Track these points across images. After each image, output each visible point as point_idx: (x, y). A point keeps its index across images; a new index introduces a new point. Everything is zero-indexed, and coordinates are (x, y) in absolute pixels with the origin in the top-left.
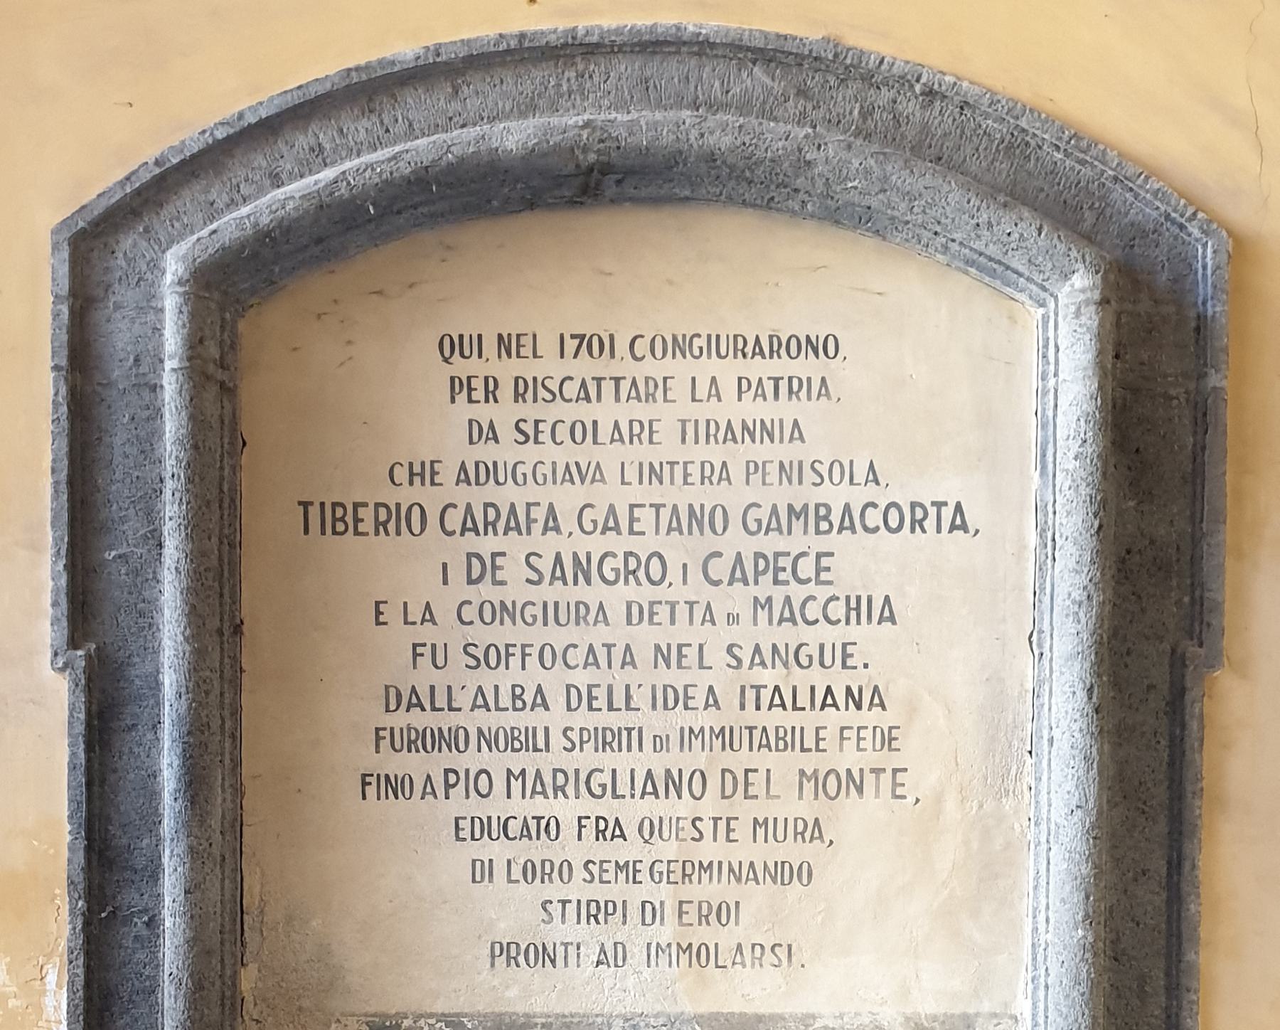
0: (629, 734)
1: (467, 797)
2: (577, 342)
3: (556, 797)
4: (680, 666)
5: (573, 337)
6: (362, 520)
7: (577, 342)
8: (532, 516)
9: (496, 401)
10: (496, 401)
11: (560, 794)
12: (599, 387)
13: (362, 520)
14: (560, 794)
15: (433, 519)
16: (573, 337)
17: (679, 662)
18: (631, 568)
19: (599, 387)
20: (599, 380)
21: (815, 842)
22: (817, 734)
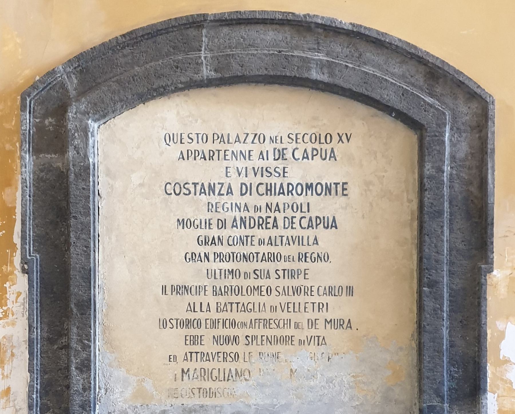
0: (336, 187)
1: (251, 184)
2: (221, 193)
3: (288, 195)
4: (249, 159)
5: (219, 184)
6: (295, 223)
7: (221, 193)
8: (228, 171)
9: (213, 160)
10: (213, 160)
11: (290, 194)
12: (191, 355)
13: (295, 223)
14: (290, 194)
15: (254, 189)
16: (219, 184)
17: (249, 157)
18: (314, 154)
19: (191, 355)
20: (191, 353)
21: (236, 143)
22: (225, 152)
